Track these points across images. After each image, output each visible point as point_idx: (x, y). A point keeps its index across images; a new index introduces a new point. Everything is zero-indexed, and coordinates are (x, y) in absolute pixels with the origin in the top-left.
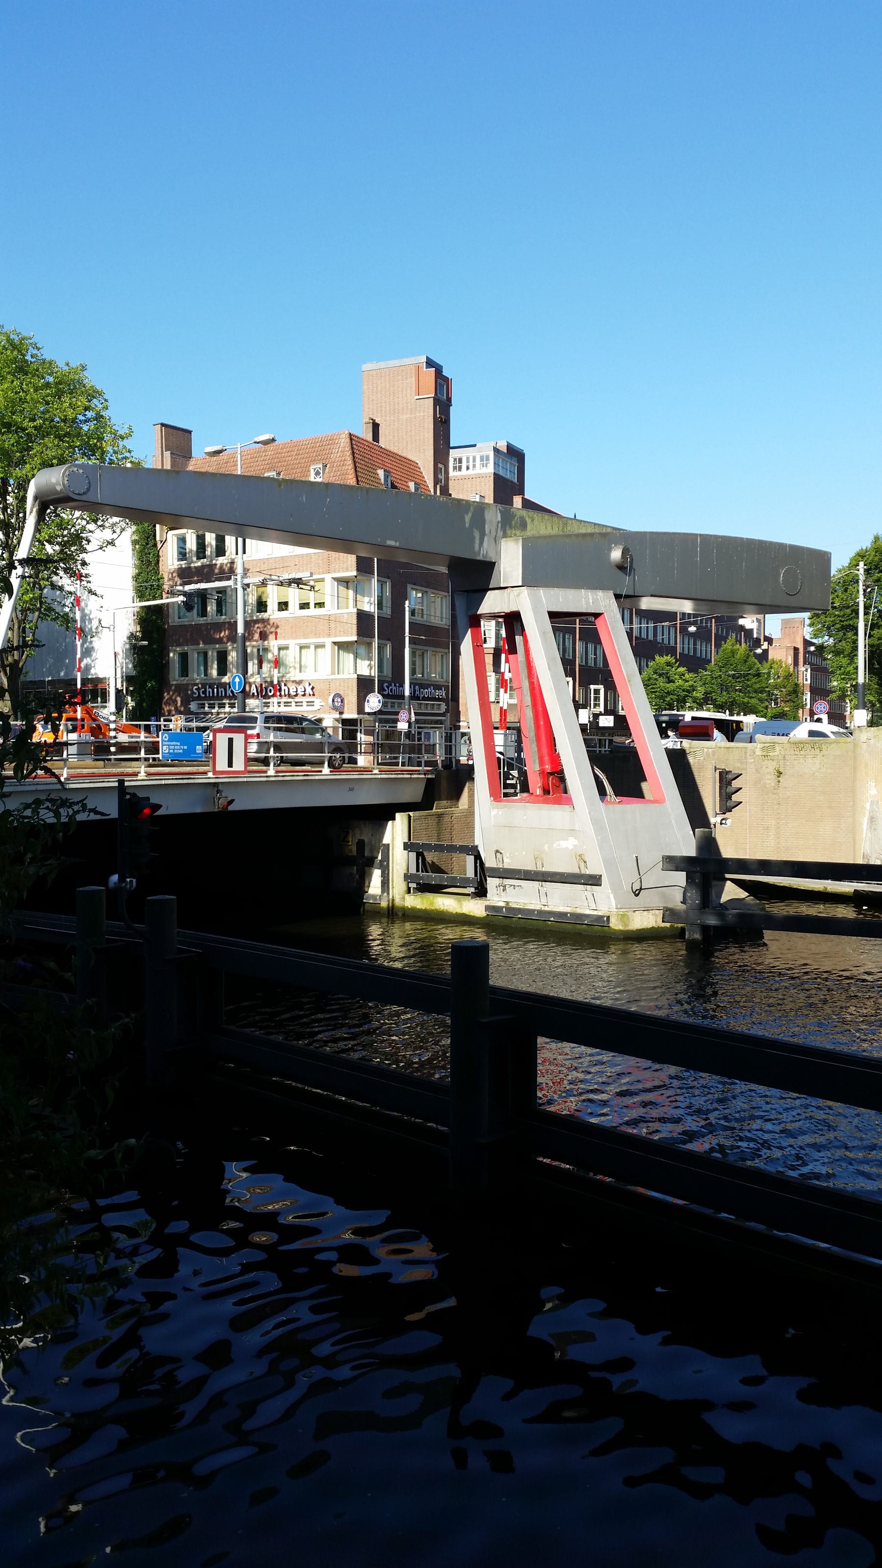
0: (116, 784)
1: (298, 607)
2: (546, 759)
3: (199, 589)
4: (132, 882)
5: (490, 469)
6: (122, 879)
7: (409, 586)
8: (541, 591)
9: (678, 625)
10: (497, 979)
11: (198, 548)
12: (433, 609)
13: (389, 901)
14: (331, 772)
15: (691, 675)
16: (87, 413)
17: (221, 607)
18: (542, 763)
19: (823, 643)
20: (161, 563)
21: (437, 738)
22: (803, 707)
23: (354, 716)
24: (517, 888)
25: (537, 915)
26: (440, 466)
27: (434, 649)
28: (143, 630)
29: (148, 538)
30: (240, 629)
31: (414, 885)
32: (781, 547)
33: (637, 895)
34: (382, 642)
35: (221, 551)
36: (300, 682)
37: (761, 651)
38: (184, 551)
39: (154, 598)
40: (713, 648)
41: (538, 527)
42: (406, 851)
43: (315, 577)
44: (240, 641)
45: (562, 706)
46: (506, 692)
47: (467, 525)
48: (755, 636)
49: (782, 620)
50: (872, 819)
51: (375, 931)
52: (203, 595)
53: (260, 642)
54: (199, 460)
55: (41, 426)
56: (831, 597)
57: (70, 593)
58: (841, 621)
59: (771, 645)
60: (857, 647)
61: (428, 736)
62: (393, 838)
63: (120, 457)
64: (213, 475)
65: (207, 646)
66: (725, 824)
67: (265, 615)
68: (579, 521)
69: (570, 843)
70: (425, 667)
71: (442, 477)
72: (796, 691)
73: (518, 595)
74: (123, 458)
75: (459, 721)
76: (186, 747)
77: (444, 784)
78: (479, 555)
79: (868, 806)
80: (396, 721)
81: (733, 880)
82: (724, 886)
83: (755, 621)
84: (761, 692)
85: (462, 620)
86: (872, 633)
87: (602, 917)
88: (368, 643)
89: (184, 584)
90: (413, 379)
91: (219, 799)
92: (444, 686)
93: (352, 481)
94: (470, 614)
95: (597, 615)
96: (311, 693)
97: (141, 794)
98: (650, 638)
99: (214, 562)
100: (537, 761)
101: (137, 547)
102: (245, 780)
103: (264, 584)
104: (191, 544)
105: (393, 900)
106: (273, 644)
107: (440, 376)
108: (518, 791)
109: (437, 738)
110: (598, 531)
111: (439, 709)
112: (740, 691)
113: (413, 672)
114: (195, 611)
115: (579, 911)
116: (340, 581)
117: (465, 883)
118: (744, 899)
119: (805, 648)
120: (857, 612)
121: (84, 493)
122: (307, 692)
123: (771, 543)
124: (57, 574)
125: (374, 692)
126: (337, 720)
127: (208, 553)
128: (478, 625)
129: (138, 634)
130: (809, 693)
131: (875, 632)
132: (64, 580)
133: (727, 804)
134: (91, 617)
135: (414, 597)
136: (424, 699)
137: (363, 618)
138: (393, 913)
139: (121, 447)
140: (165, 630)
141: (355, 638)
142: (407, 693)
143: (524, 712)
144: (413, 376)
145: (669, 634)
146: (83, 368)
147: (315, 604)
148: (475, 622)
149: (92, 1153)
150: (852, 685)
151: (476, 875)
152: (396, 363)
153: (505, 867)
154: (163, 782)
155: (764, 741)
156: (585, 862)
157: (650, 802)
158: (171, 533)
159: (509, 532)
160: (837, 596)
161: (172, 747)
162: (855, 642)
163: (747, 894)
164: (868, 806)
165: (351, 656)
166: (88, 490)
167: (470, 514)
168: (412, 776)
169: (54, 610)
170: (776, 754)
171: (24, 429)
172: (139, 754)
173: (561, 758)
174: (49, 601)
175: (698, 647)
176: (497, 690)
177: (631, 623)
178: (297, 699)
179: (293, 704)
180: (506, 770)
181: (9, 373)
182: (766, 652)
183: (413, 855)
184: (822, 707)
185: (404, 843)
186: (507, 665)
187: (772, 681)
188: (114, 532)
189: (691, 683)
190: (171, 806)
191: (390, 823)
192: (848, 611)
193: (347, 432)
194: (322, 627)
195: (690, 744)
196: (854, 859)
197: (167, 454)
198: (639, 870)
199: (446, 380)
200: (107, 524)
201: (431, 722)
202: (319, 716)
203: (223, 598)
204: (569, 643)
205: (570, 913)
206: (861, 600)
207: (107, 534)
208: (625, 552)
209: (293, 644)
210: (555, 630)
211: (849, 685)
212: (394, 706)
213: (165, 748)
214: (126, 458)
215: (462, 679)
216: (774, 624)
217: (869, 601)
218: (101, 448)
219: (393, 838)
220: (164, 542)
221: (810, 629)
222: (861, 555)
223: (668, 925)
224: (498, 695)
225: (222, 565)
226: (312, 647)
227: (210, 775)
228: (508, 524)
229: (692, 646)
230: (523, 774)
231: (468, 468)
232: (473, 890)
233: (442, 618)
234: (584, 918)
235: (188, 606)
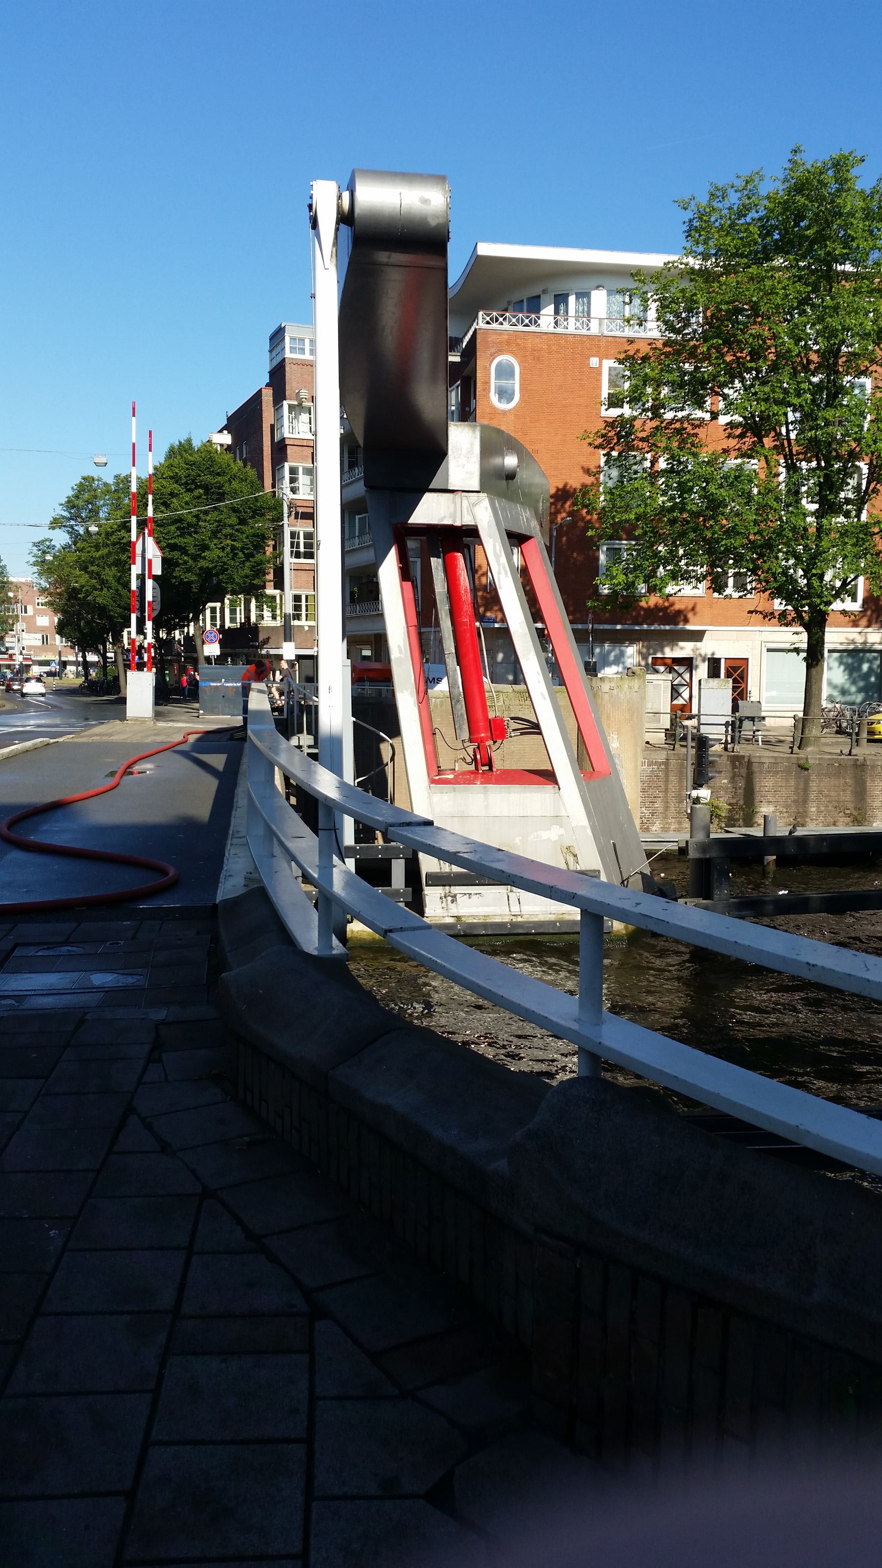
24: (473, 897)
156: (575, 856)
198: (619, 865)
215: (306, 523)
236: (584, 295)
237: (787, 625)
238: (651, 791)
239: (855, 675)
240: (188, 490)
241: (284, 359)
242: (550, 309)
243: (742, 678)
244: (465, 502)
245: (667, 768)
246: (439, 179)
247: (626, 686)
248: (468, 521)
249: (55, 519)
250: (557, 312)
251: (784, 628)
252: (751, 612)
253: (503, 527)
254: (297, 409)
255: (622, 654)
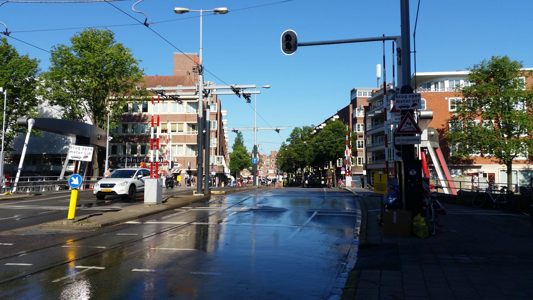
1: (171, 131)
116: (188, 124)
194: (182, 139)
226: (177, 146)
236: (443, 82)
237: (501, 164)
239: (527, 177)
240: (333, 132)
241: (356, 98)
242: (433, 86)
243: (493, 179)
244: (425, 142)
246: (432, 110)
248: (425, 146)
249: (287, 139)
250: (435, 87)
251: (500, 165)
252: (491, 161)
253: (433, 147)
254: (360, 110)
255: (457, 172)
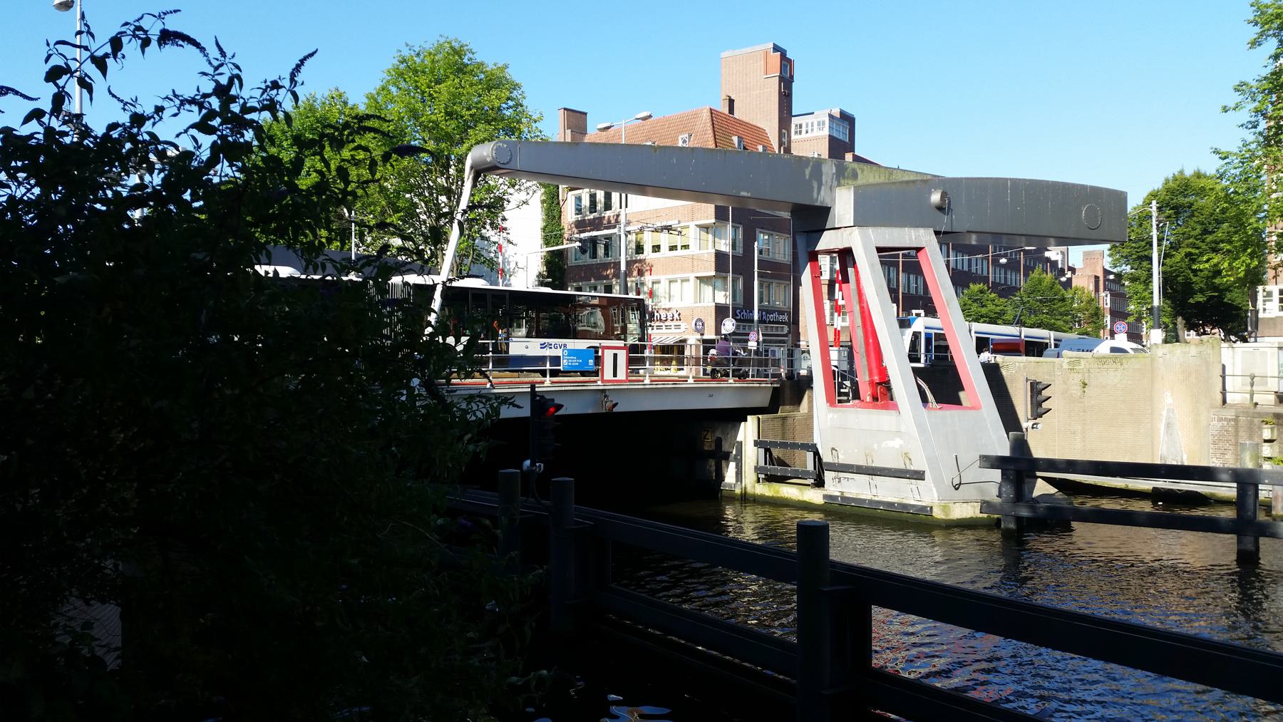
0: (529, 390)
2: (875, 371)
3: (591, 236)
4: (540, 466)
5: (826, 132)
6: (533, 464)
7: (758, 230)
8: (870, 230)
9: (990, 257)
10: (835, 555)
11: (590, 205)
12: (777, 248)
13: (742, 489)
14: (695, 381)
15: (1001, 300)
16: (509, 101)
17: (608, 250)
18: (871, 374)
19: (1121, 272)
20: (562, 217)
21: (781, 353)
22: (1104, 328)
23: (713, 337)
25: (868, 504)
26: (784, 131)
27: (778, 281)
28: (549, 270)
29: (553, 198)
30: (623, 267)
31: (763, 476)
32: (1082, 188)
33: (957, 489)
34: (736, 276)
35: (608, 206)
36: (668, 310)
37: (1066, 279)
38: (580, 207)
39: (557, 245)
40: (1022, 277)
41: (867, 177)
42: (756, 448)
43: (682, 224)
44: (622, 276)
45: (889, 326)
46: (839, 315)
47: (807, 177)
48: (1060, 266)
49: (1084, 252)
50: (1169, 425)
51: (730, 513)
52: (594, 241)
53: (638, 277)
54: (592, 135)
55: (475, 114)
56: (1128, 230)
57: (495, 243)
58: (1137, 252)
59: (1075, 274)
60: (1152, 274)
61: (774, 352)
62: (745, 437)
63: (533, 135)
64: (604, 144)
65: (597, 282)
66: (1037, 428)
67: (641, 257)
68: (902, 170)
69: (897, 443)
70: (771, 295)
71: (785, 140)
72: (1097, 315)
73: (850, 234)
74: (535, 136)
75: (799, 341)
76: (581, 361)
77: (788, 393)
78: (817, 201)
79: (1164, 413)
80: (747, 341)
81: (1043, 478)
82: (1035, 483)
83: (1060, 253)
84: (1066, 315)
85: (802, 256)
86: (1165, 261)
87: (926, 507)
88: (724, 277)
89: (580, 232)
90: (762, 62)
91: (606, 402)
92: (786, 312)
93: (711, 145)
94: (809, 250)
95: (919, 249)
96: (678, 318)
97: (548, 397)
98: (965, 269)
99: (603, 215)
100: (867, 373)
101: (545, 205)
102: (626, 387)
103: (641, 230)
104: (586, 202)
105: (745, 488)
106: (648, 279)
107: (784, 58)
108: (850, 398)
109: (781, 353)
110: (920, 179)
111: (782, 331)
112: (1047, 313)
113: (761, 300)
114: (588, 253)
115: (905, 501)
116: (701, 227)
117: (805, 475)
118: (1053, 494)
119: (1105, 277)
120: (1151, 244)
121: (508, 163)
122: (675, 318)
123: (1074, 185)
124: (485, 228)
125: (729, 317)
126: (699, 340)
127: (598, 208)
128: (816, 260)
129: (544, 273)
130: (1109, 316)
131: (1168, 261)
132: (489, 232)
133: (1038, 410)
134: (510, 260)
135: (762, 238)
136: (770, 322)
137: (720, 257)
138: (745, 498)
139: (534, 128)
140: (565, 270)
141: (713, 273)
142: (756, 318)
143: (856, 332)
144: (762, 59)
145: (982, 265)
146: (506, 67)
147: (682, 246)
148: (813, 257)
149: (514, 678)
150: (1147, 309)
151: (815, 468)
152: (749, 50)
153: (840, 462)
154: (563, 388)
155: (1070, 356)
156: (910, 459)
157: (967, 408)
158: (571, 193)
159: (842, 182)
160: (1133, 231)
161: (570, 361)
162: (1150, 270)
163: (1057, 490)
164: (1164, 413)
165: (711, 288)
166: (510, 160)
167: (810, 168)
168: (761, 385)
169: (482, 256)
170: (1081, 367)
171: (462, 117)
172: (546, 366)
173: (888, 370)
174: (479, 249)
175: (1009, 276)
176: (832, 315)
177: (948, 256)
178: (667, 323)
179: (664, 327)
180: (840, 380)
181: (451, 73)
182: (1070, 280)
183: (762, 451)
184: (1121, 326)
185: (755, 441)
186: (840, 293)
187: (1076, 305)
188: (528, 194)
189: (1001, 308)
190: (571, 408)
191: (743, 423)
192: (1143, 244)
193: (708, 108)
195: (1003, 359)
196: (1153, 460)
197: (569, 132)
199: (790, 61)
200: (522, 188)
201: (776, 342)
202: (684, 337)
203: (609, 243)
204: (893, 275)
205: (897, 503)
206: (1155, 233)
207: (523, 196)
208: (944, 195)
209: (664, 279)
210: (882, 263)
211: (1145, 309)
212: (745, 329)
213: (565, 361)
214: (538, 136)
216: (1076, 255)
217: (1161, 235)
218: (519, 129)
219: (745, 437)
220: (564, 201)
221: (1110, 259)
222: (1154, 195)
223: (985, 516)
224: (832, 319)
225: (609, 217)
226: (679, 281)
227: (599, 383)
228: (842, 175)
229: (1003, 276)
230: (855, 386)
231: (807, 132)
232: (812, 481)
233: (785, 255)
234: (910, 508)
235: (583, 250)
238: (1221, 444)
245: (1237, 424)
247: (1179, 351)
